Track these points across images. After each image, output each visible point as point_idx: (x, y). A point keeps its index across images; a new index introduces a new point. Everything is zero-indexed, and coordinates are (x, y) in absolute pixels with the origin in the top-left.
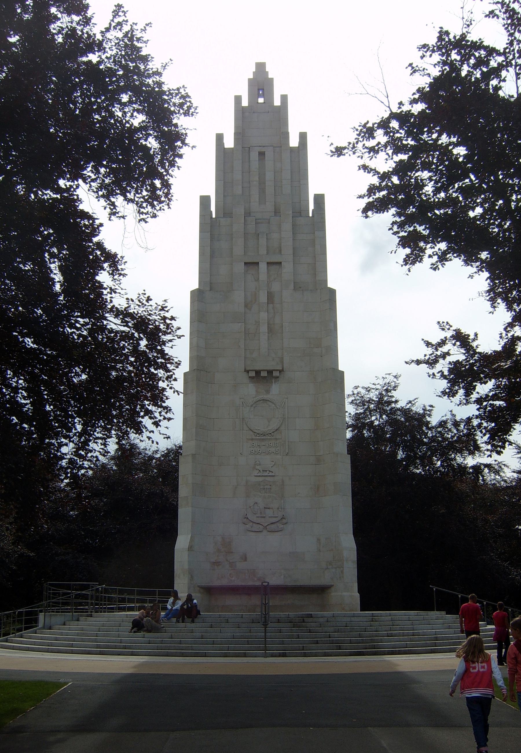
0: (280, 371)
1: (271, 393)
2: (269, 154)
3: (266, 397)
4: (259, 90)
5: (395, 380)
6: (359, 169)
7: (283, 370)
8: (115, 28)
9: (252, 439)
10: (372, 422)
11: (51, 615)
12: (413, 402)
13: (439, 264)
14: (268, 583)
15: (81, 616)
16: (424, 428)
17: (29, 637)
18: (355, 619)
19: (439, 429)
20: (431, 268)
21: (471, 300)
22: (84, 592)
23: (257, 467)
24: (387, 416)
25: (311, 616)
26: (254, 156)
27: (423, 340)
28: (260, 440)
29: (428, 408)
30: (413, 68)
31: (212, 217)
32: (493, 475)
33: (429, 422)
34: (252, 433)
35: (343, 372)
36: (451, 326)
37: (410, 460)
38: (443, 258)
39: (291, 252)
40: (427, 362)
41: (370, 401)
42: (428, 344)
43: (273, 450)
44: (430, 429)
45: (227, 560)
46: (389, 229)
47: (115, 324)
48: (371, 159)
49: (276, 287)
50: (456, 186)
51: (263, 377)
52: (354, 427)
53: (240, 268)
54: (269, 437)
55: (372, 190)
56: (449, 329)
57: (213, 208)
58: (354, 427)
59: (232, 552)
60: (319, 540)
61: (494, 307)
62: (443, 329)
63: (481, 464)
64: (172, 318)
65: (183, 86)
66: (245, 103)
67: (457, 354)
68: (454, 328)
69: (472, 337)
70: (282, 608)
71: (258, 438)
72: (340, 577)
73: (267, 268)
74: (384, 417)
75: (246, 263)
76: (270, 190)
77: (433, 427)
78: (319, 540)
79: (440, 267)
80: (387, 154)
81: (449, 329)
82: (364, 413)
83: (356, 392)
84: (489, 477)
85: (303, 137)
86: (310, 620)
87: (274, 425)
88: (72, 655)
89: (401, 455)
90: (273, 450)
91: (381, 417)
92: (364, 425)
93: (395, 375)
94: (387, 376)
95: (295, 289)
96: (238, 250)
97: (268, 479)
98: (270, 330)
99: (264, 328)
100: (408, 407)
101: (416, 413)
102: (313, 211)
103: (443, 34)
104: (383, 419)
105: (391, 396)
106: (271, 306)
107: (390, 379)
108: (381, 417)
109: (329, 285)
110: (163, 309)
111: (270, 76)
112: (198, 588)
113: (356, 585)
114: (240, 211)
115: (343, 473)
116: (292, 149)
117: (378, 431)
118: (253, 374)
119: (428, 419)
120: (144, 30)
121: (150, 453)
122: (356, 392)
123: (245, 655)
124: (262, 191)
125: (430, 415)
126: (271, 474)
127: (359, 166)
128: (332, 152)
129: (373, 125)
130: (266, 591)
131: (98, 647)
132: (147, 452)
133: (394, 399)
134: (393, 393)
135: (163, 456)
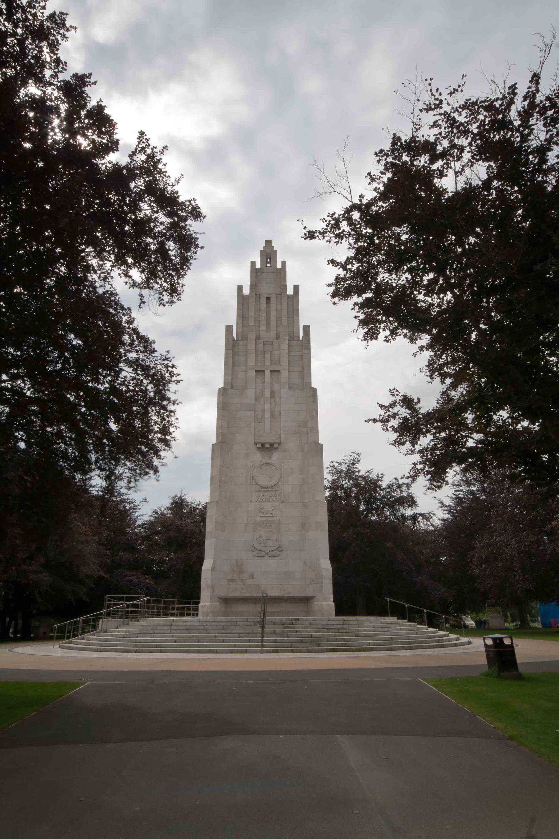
0: (279, 444)
2: (273, 300)
3: (269, 461)
4: (267, 258)
5: (358, 457)
6: (329, 264)
8: (140, 152)
9: (259, 491)
10: (343, 485)
13: (390, 338)
16: (378, 489)
17: (90, 638)
18: (330, 622)
19: (388, 490)
20: (385, 340)
26: (263, 300)
27: (378, 404)
28: (264, 491)
29: (380, 476)
30: (371, 176)
31: (234, 340)
32: (425, 521)
33: (381, 486)
35: (322, 445)
36: (400, 393)
37: (369, 510)
38: (393, 333)
39: (287, 364)
40: (381, 421)
41: (342, 471)
42: (381, 406)
43: (273, 498)
44: (381, 490)
46: (352, 309)
47: (128, 372)
48: (337, 245)
49: (276, 387)
50: (405, 268)
51: (266, 448)
53: (252, 373)
55: (338, 280)
56: (398, 395)
57: (235, 335)
58: (331, 488)
61: (433, 378)
62: (393, 395)
63: (417, 513)
64: (173, 366)
65: (194, 199)
66: (258, 266)
67: (404, 412)
68: (402, 394)
69: (416, 400)
70: (270, 613)
74: (351, 481)
75: (256, 371)
77: (384, 489)
78: (305, 563)
79: (392, 340)
80: (350, 244)
81: (398, 395)
82: (338, 479)
84: (422, 524)
85: (296, 288)
87: (274, 481)
89: (362, 507)
90: (273, 498)
91: (349, 481)
92: (338, 488)
94: (353, 454)
95: (289, 388)
96: (251, 361)
97: (270, 519)
98: (272, 416)
99: (268, 415)
100: (367, 475)
101: (372, 479)
103: (396, 140)
106: (273, 400)
108: (349, 481)
109: (313, 386)
110: (166, 359)
111: (275, 249)
114: (252, 336)
115: (323, 516)
116: (289, 296)
117: (348, 493)
118: (260, 446)
119: (381, 483)
120: (162, 152)
121: (194, 505)
122: (332, 465)
123: (247, 652)
125: (381, 481)
127: (328, 261)
128: (305, 234)
129: (339, 215)
130: (266, 600)
131: (136, 646)
132: (193, 505)
133: (357, 470)
134: (357, 466)
135: (203, 507)
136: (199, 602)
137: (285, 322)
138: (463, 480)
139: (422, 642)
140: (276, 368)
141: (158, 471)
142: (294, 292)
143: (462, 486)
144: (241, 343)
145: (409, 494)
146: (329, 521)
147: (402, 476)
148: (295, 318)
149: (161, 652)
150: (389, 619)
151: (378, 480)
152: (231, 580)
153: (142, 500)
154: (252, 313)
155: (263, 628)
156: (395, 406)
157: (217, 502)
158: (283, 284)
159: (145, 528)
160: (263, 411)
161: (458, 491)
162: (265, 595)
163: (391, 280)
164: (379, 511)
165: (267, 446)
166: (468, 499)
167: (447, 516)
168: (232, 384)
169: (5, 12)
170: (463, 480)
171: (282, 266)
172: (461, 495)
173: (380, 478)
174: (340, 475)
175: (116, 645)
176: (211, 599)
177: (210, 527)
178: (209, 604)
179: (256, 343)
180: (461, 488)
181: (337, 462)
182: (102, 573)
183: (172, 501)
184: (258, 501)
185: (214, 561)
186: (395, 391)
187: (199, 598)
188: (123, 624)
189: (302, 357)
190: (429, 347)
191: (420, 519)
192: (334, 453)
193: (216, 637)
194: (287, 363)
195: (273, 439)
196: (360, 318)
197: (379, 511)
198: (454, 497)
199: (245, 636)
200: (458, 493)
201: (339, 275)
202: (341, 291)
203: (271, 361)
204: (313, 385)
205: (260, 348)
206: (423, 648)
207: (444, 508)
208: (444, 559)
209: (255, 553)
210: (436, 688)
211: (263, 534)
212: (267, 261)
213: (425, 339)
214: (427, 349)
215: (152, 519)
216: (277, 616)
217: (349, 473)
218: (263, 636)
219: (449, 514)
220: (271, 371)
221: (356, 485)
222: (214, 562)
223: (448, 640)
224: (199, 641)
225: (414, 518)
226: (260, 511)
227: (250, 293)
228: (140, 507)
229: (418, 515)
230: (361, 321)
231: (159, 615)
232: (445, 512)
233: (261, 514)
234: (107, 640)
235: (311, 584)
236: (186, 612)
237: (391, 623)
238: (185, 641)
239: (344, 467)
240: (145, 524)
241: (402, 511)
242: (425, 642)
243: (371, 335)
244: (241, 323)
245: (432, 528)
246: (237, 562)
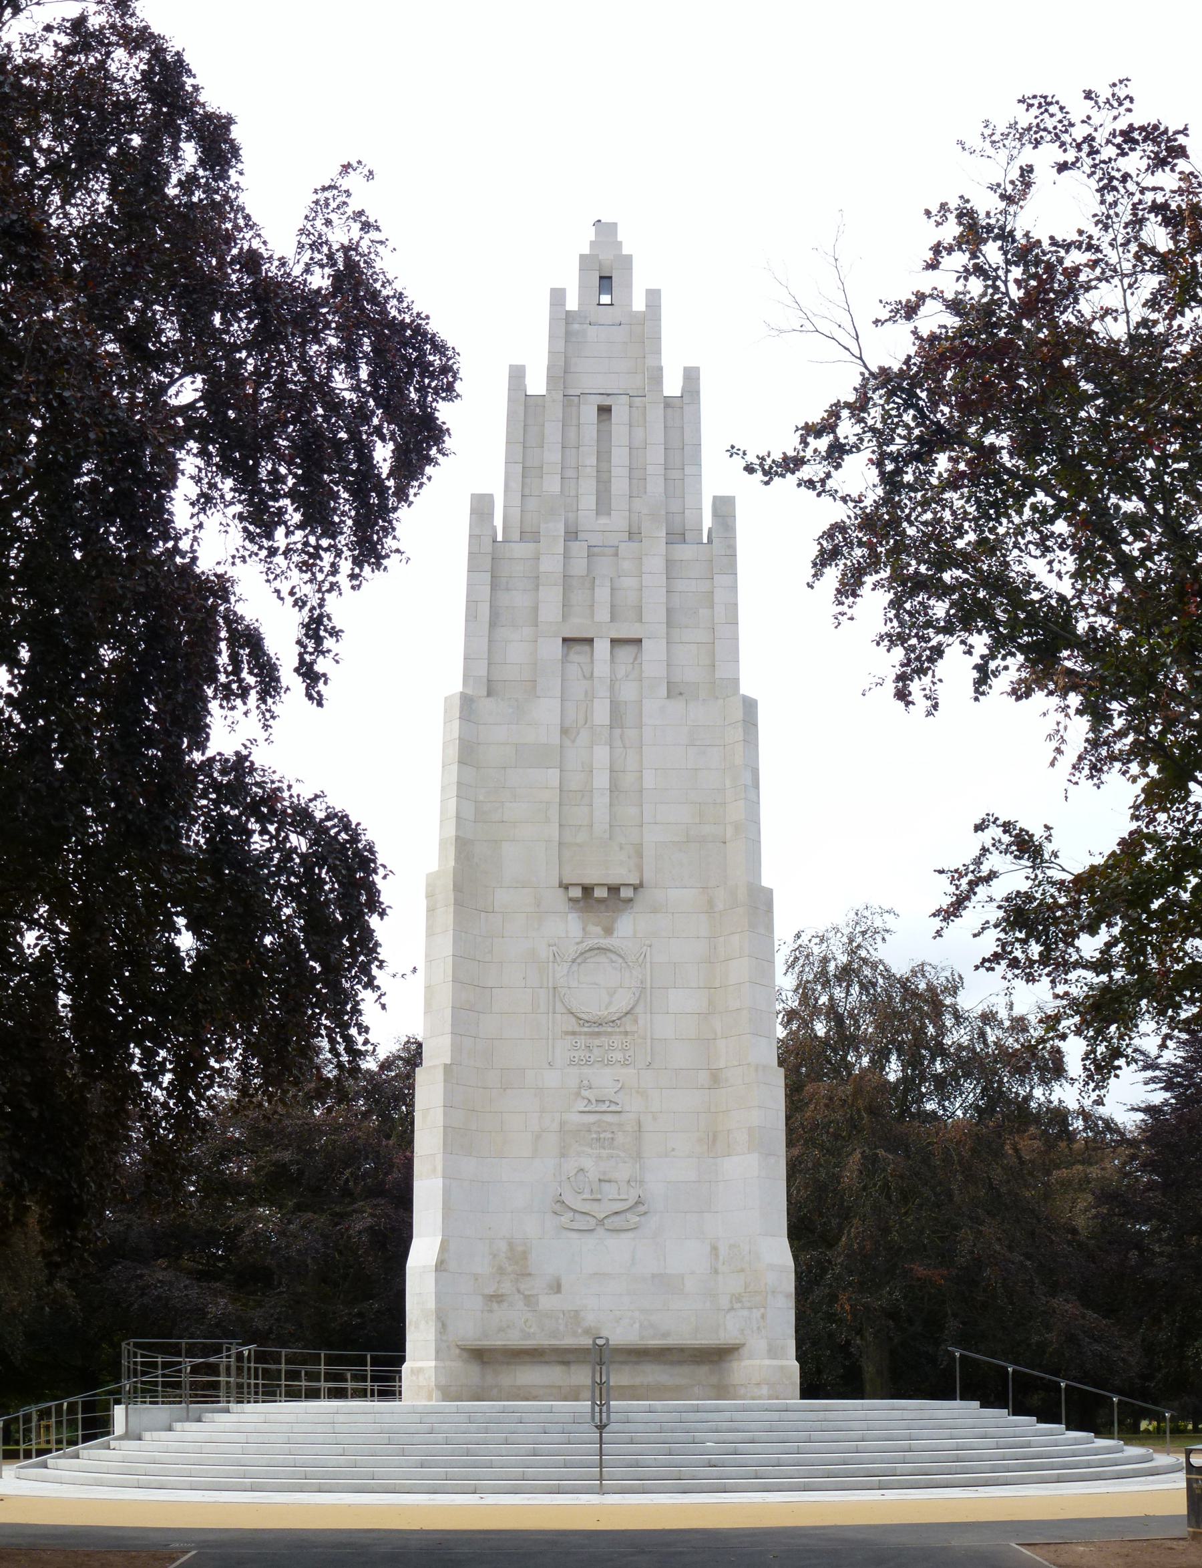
0: (636, 888)
1: (615, 935)
2: (620, 413)
3: (604, 942)
7: (641, 885)
9: (574, 1033)
14: (607, 1340)
22: (211, 1360)
23: (585, 1093)
26: (590, 413)
34: (574, 1020)
35: (771, 891)
43: (618, 1056)
45: (519, 1291)
49: (628, 692)
51: (599, 900)
57: (498, 521)
59: (530, 1274)
60: (715, 1249)
66: (572, 304)
71: (586, 1029)
72: (758, 1328)
76: (620, 486)
78: (715, 1249)
85: (691, 377)
87: (622, 1002)
96: (550, 611)
97: (609, 1118)
99: (601, 780)
102: (710, 531)
106: (617, 732)
111: (625, 251)
112: (458, 1351)
113: (792, 1344)
116: (668, 403)
118: (576, 893)
126: (613, 1108)
136: (402, 1360)
137: (655, 487)
144: (521, 550)
148: (688, 470)
152: (497, 1298)
154: (553, 455)
165: (600, 893)
167: (1159, 1097)
169: (312, 963)
184: (572, 1063)
189: (709, 599)
195: (620, 873)
204: (746, 689)
205: (579, 566)
207: (1149, 1074)
209: (565, 1219)
211: (588, 1163)
219: (1166, 1089)
220: (614, 641)
235: (732, 1309)
244: (516, 485)
246: (511, 1246)
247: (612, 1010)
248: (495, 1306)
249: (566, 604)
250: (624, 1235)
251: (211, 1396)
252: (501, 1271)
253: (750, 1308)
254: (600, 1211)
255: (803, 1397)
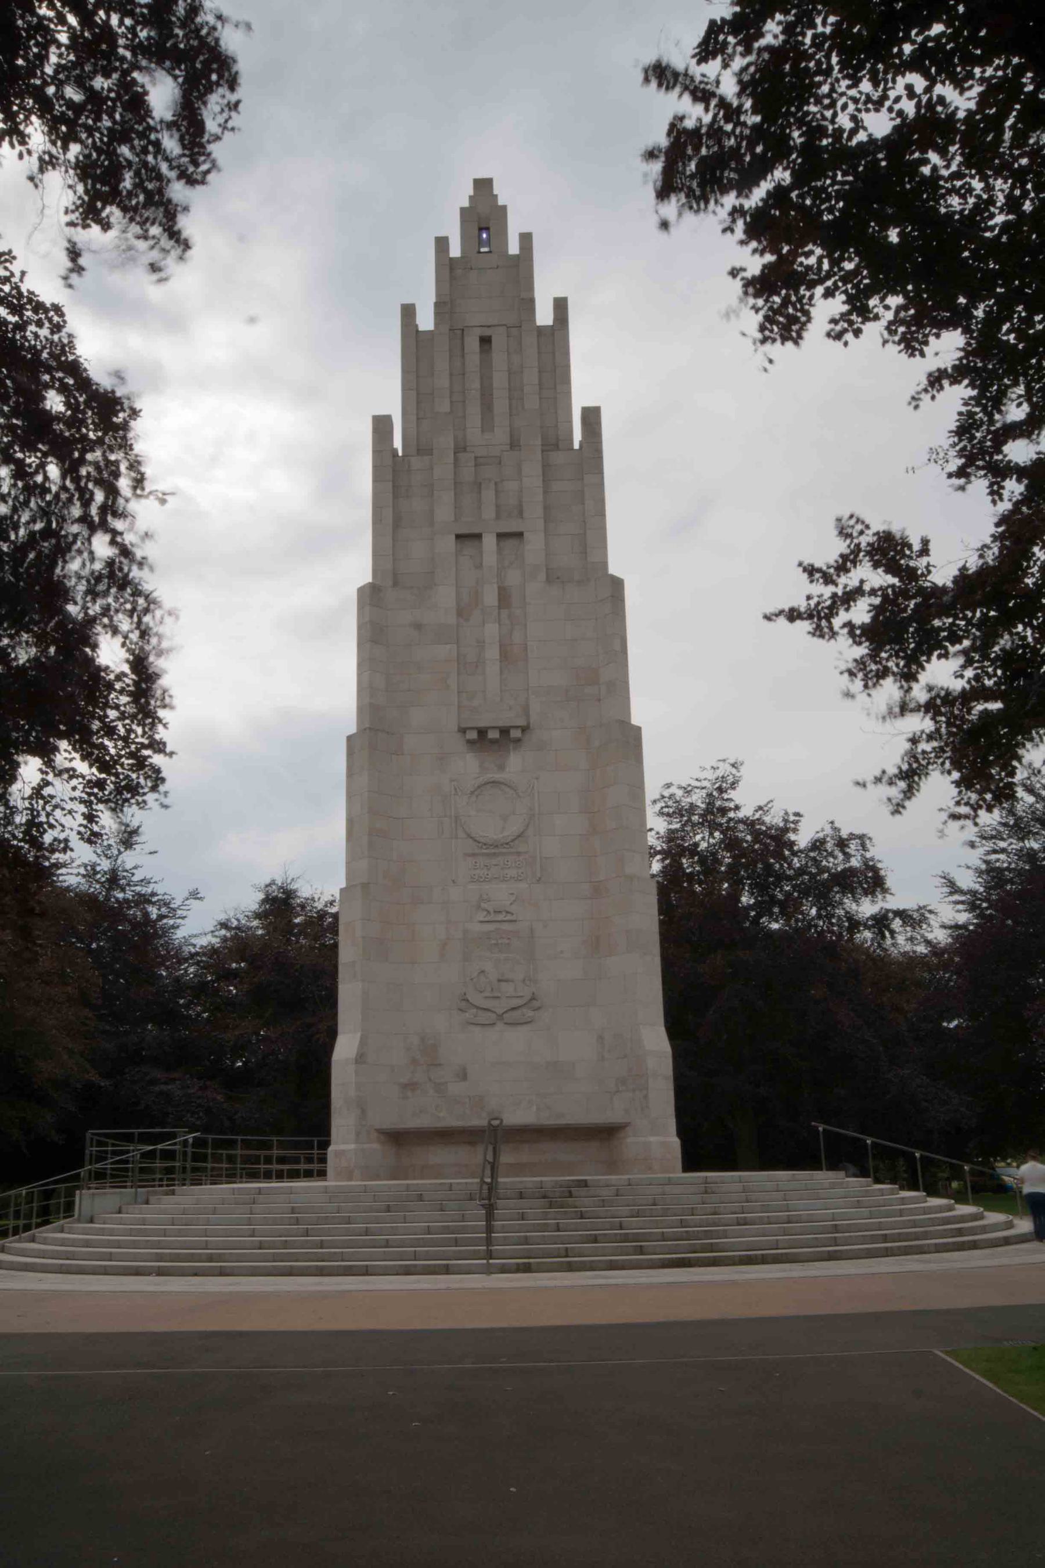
0: (524, 729)
3: (498, 776)
5: (734, 771)
6: (647, 80)
9: (474, 855)
11: (93, 1194)
12: (766, 809)
15: (155, 1193)
16: (787, 853)
17: (52, 1237)
19: (812, 854)
20: (829, 335)
21: (911, 472)
24: (722, 832)
25: (584, 1184)
26: (472, 344)
28: (488, 855)
29: (792, 818)
33: (792, 843)
35: (639, 729)
37: (764, 908)
41: (692, 807)
42: (811, 571)
44: (794, 854)
45: (430, 1080)
46: (724, 231)
49: (513, 578)
51: (491, 740)
52: (666, 854)
54: (504, 850)
57: (398, 443)
58: (666, 854)
59: (440, 1065)
63: (888, 911)
66: (455, 251)
69: (917, 547)
70: (508, 1166)
73: (498, 545)
75: (458, 537)
77: (801, 851)
78: (601, 1038)
83: (666, 793)
84: (902, 942)
85: (561, 306)
86: (583, 1191)
87: (514, 828)
88: (130, 1270)
89: (746, 899)
91: (711, 834)
92: (682, 851)
93: (732, 761)
94: (721, 764)
95: (549, 580)
96: (444, 513)
97: (505, 927)
98: (505, 656)
99: (492, 653)
100: (757, 816)
104: (714, 838)
105: (727, 800)
106: (505, 613)
107: (725, 769)
111: (500, 203)
112: (376, 1134)
114: (446, 442)
115: (645, 917)
116: (541, 331)
117: (708, 861)
118: (473, 735)
119: (792, 837)
121: (319, 905)
123: (447, 1270)
124: (487, 406)
126: (509, 917)
130: (496, 1136)
131: (160, 1258)
132: (316, 904)
133: (732, 805)
134: (732, 794)
138: (1005, 825)
139: (917, 1237)
140: (513, 526)
141: (163, 780)
142: (555, 319)
143: (1003, 839)
144: (416, 463)
145: (866, 862)
146: (661, 934)
147: (878, 773)
149: (222, 1273)
150: (823, 1177)
151: (785, 830)
153: (186, 894)
154: (443, 382)
155: (490, 1211)
156: (854, 563)
157: (365, 886)
158: (524, 295)
159: (198, 963)
160: (481, 644)
161: (995, 852)
162: (496, 1123)
163: (856, 101)
164: (789, 908)
165: (493, 735)
166: (1020, 872)
167: (963, 918)
168: (395, 575)
170: (1005, 825)
171: (521, 248)
172: (1002, 860)
173: (791, 823)
174: (689, 820)
175: (110, 1257)
176: (358, 1134)
177: (347, 954)
178: (352, 1146)
179: (456, 460)
180: (1003, 844)
181: (680, 787)
182: (93, 1076)
183: (262, 896)
185: (361, 1038)
186: (852, 522)
187: (327, 1133)
188: (136, 1203)
190: (958, 374)
191: (897, 924)
192: (673, 760)
193: (367, 1232)
194: (539, 511)
196: (748, 274)
197: (789, 908)
198: (984, 867)
199: (447, 1230)
200: (994, 857)
201: (682, 118)
202: (692, 168)
203: (498, 506)
204: (613, 570)
205: (468, 473)
206: (921, 1251)
208: (952, 1025)
210: (995, 1383)
212: (480, 236)
213: (948, 346)
214: (955, 381)
215: (215, 941)
216: (524, 1174)
217: (712, 813)
218: (489, 1229)
221: (731, 843)
222: (363, 1042)
223: (984, 1229)
224: (321, 1245)
225: (881, 922)
226: (479, 907)
227: (436, 324)
228: (184, 913)
229: (891, 915)
230: (748, 283)
231: (234, 1175)
232: (961, 907)
233: (481, 916)
234: (87, 1244)
236: (303, 1167)
237: (833, 1186)
238: (285, 1245)
239: (698, 799)
240: (197, 954)
241: (849, 904)
242: (926, 1236)
243: (785, 325)
245: (922, 949)
247: (506, 834)
248: (409, 1094)
249: (457, 507)
250: (519, 1028)
251: (148, 1181)
252: (414, 1061)
253: (634, 1090)
254: (500, 1006)
255: (686, 1169)
